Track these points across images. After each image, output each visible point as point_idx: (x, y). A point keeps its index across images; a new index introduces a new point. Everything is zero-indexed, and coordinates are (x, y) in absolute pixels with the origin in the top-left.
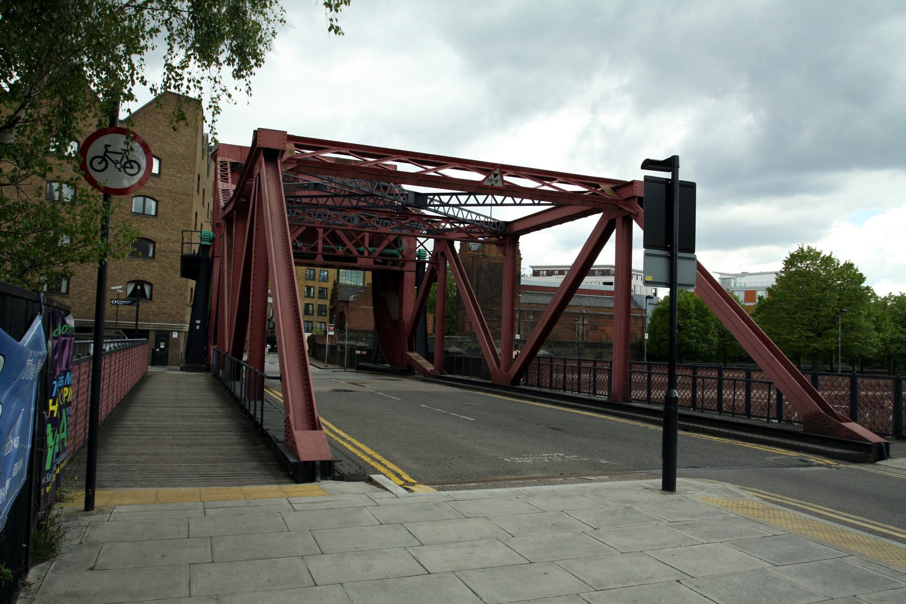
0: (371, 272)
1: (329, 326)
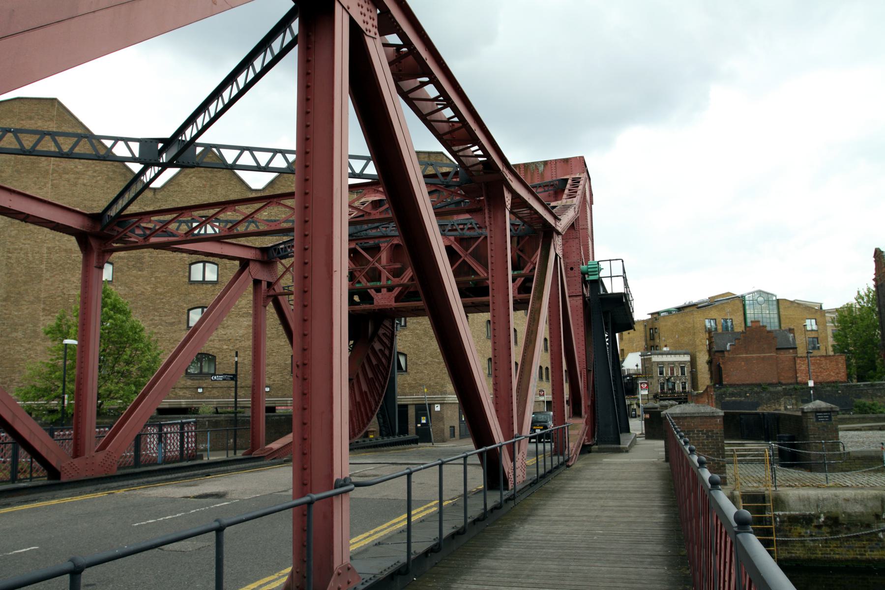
0: (216, 279)
1: (641, 383)
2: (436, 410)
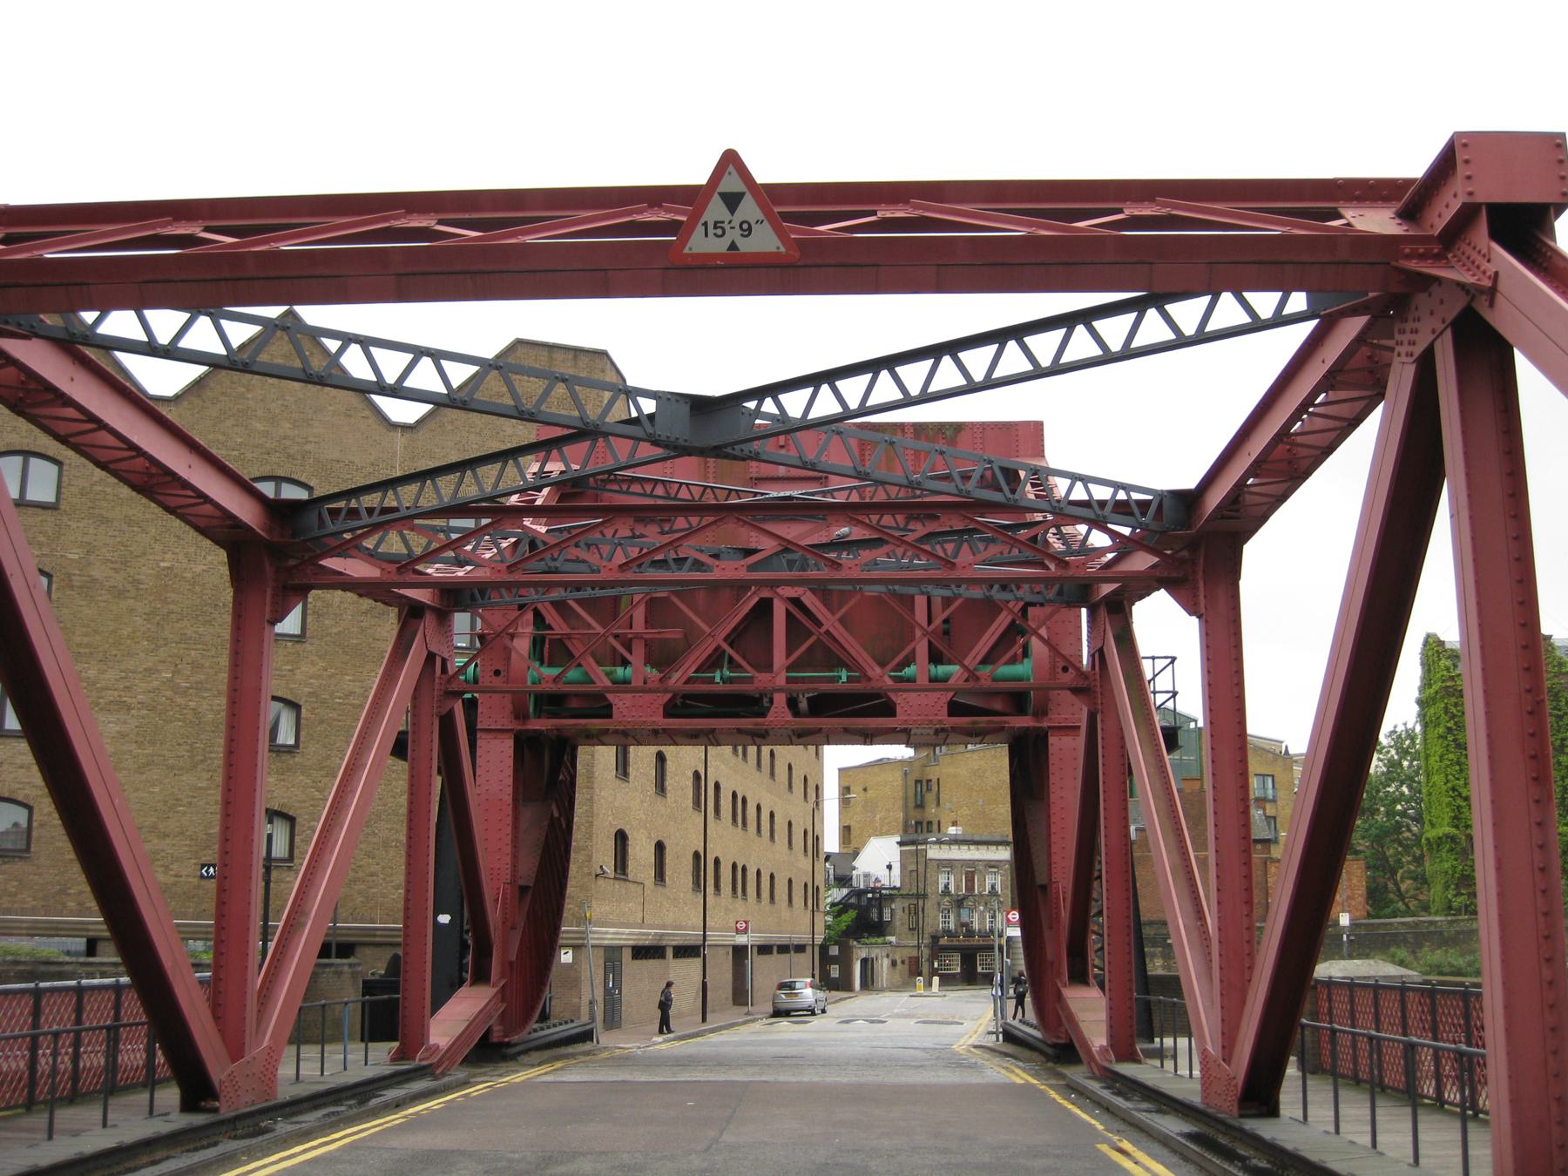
2: (563, 961)
